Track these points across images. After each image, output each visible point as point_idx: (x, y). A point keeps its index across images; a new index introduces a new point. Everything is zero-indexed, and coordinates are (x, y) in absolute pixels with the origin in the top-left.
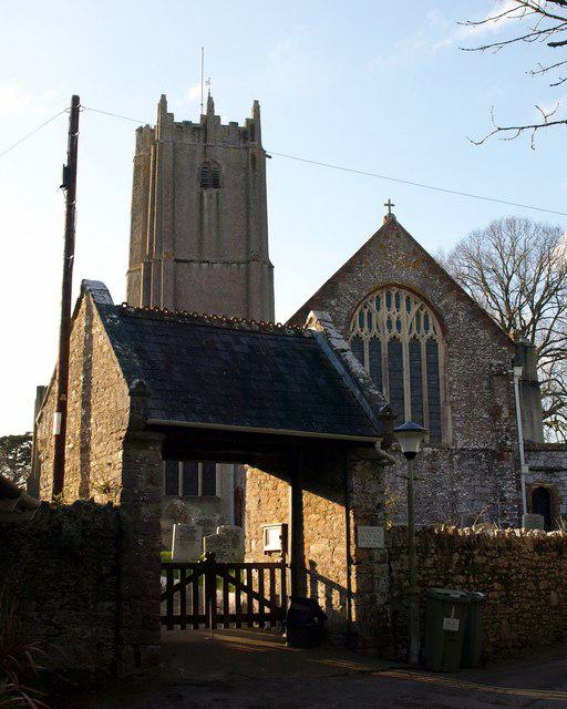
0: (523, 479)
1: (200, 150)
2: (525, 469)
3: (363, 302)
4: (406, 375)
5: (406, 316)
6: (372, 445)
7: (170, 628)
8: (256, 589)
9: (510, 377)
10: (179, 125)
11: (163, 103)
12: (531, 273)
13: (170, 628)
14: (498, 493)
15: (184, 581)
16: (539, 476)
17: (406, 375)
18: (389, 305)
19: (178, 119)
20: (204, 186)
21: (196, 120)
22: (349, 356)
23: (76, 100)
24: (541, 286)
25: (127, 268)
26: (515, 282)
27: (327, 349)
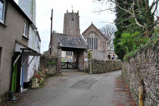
0: (107, 54)
1: (71, 16)
2: (107, 53)
3: (89, 34)
4: (94, 42)
5: (94, 35)
6: (86, 49)
7: (63, 69)
8: (72, 66)
9: (106, 42)
10: (69, 13)
11: (67, 11)
12: (111, 31)
13: (63, 69)
14: (104, 55)
15: (65, 64)
16: (109, 54)
17: (94, 42)
18: (92, 34)
19: (69, 12)
20: (72, 20)
21: (71, 13)
22: (84, 39)
23: (52, 9)
24: (112, 32)
25: (63, 30)
26: (109, 32)
27: (82, 38)
